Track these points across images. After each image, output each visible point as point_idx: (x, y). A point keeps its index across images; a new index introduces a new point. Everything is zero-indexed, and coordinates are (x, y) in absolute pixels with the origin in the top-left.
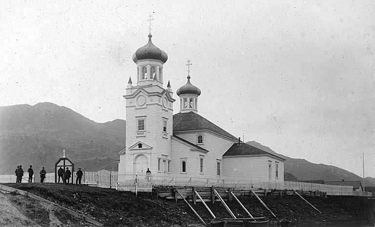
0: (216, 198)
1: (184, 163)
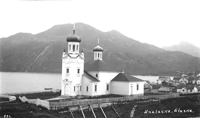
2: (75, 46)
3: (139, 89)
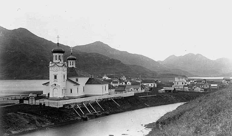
0: (84, 105)
1: (71, 90)
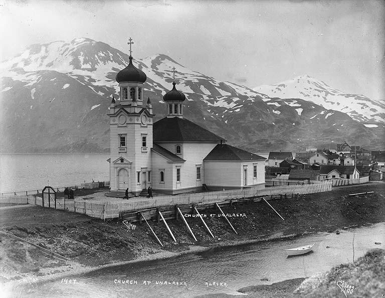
1: (162, 173)
2: (134, 89)
3: (181, 178)
